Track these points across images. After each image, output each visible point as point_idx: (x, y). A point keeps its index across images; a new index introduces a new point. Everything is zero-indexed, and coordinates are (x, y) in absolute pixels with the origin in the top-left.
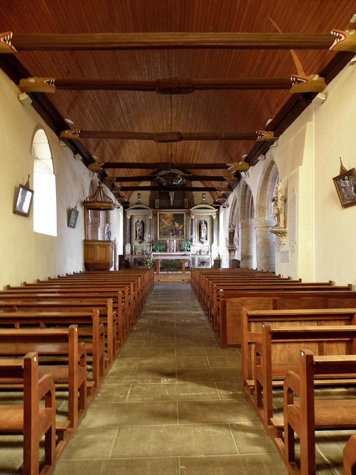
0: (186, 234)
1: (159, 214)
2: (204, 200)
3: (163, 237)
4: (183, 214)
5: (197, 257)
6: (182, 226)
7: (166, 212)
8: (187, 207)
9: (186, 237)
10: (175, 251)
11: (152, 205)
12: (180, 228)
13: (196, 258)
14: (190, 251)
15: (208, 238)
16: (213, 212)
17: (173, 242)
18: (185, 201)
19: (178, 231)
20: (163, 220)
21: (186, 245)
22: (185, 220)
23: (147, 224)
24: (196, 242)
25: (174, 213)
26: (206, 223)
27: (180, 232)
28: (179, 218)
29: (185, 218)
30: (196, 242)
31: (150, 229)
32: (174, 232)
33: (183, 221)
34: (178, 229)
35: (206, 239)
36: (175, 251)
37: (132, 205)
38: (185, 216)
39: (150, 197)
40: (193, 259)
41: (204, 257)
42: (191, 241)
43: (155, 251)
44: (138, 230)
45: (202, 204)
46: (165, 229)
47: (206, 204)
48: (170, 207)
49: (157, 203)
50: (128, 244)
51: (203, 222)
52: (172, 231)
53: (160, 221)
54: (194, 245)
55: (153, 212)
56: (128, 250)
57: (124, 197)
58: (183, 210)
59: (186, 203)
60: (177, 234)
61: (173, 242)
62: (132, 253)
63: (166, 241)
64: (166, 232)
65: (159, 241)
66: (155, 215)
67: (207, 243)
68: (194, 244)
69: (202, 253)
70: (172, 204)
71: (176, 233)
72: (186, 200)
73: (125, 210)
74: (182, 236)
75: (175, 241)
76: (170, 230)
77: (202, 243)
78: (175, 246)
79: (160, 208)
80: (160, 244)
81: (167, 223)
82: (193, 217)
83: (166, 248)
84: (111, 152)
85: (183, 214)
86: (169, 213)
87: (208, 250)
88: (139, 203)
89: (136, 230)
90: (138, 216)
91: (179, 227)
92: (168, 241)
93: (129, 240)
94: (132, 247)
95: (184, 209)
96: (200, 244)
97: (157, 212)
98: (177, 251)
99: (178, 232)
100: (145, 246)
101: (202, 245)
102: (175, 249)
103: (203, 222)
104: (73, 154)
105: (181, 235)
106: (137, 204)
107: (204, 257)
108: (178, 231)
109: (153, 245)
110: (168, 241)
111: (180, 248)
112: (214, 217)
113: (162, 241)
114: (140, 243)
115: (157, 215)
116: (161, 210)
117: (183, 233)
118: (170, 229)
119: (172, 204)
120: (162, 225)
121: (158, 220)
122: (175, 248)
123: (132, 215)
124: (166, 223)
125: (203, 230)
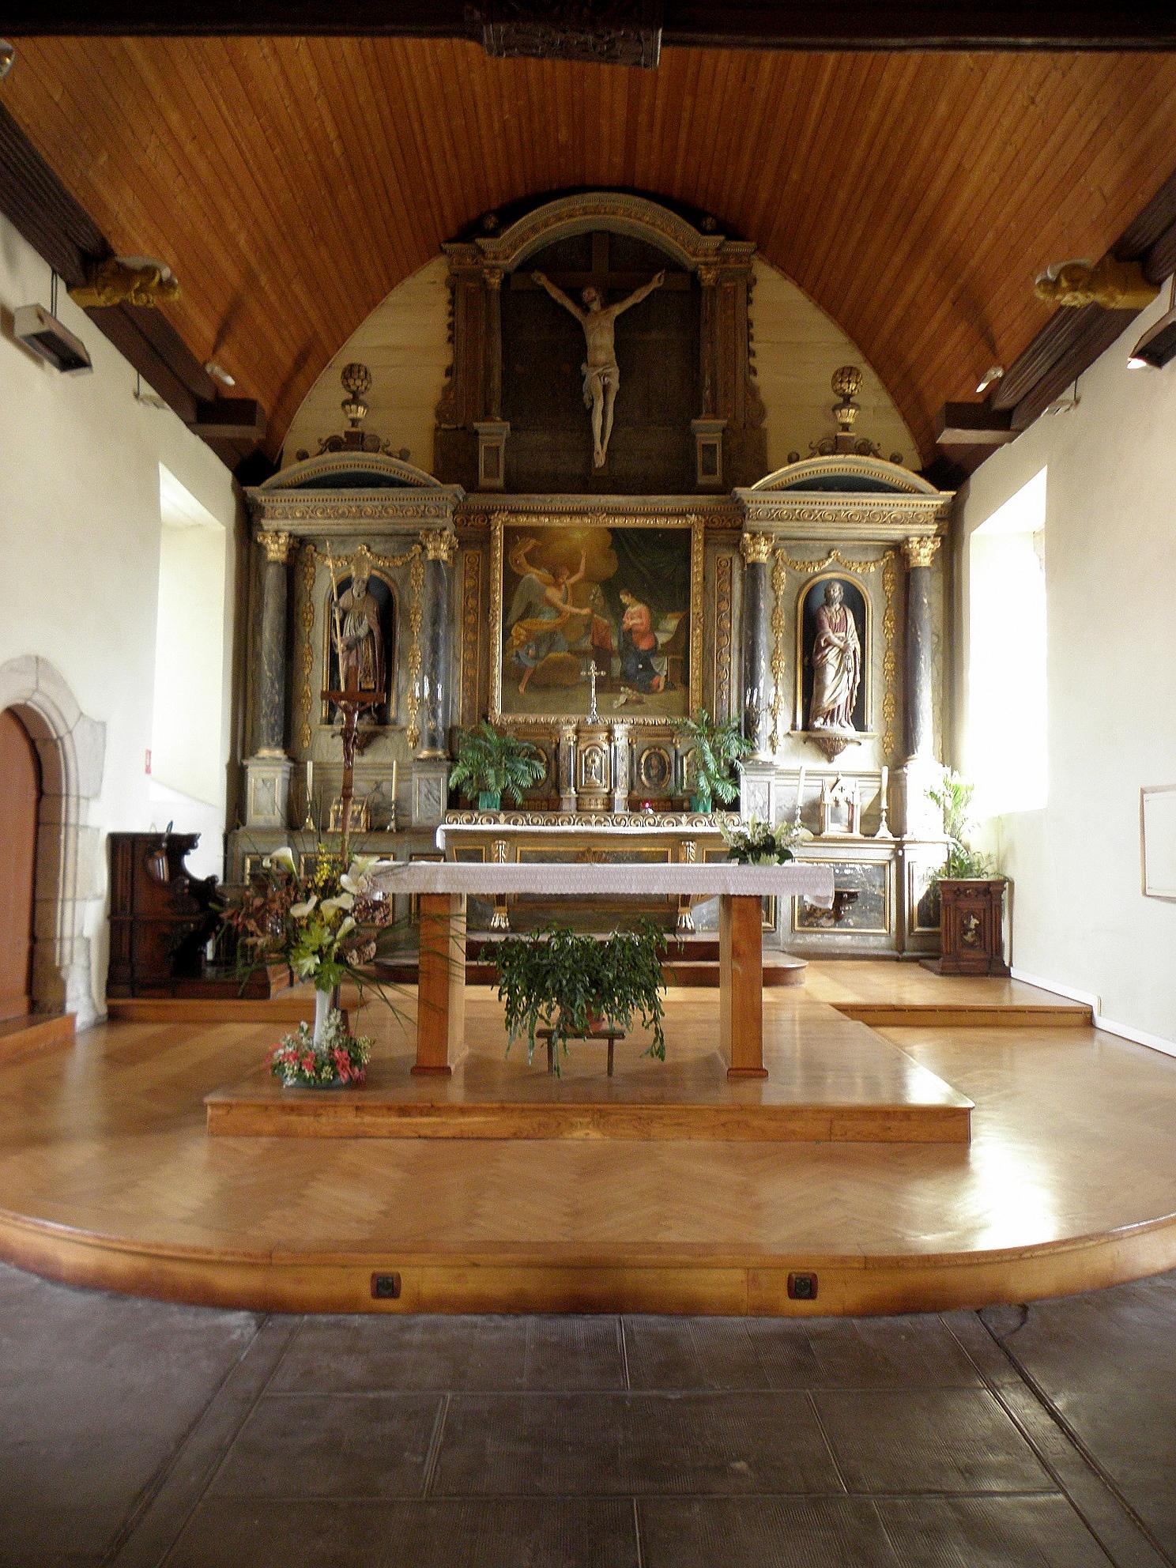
0: (706, 686)
1: (508, 531)
2: (849, 416)
3: (535, 698)
4: (687, 533)
6: (671, 624)
7: (560, 513)
8: (716, 479)
9: (706, 704)
10: (620, 809)
11: (455, 459)
12: (663, 638)
14: (734, 806)
15: (873, 714)
16: (910, 514)
17: (609, 741)
18: (702, 439)
19: (645, 658)
20: (534, 575)
21: (709, 757)
22: (696, 578)
23: (417, 601)
24: (783, 743)
25: (619, 522)
26: (855, 601)
27: (662, 667)
28: (652, 567)
29: (697, 558)
30: (783, 743)
31: (435, 641)
32: (617, 665)
33: (686, 585)
34: (644, 645)
35: (859, 722)
36: (620, 809)
37: (303, 456)
38: (697, 547)
39: (439, 414)
41: (842, 854)
42: (748, 728)
43: (472, 806)
44: (349, 648)
45: (837, 446)
46: (549, 639)
47: (865, 449)
48: (589, 483)
49: (493, 451)
50: (264, 752)
51: (837, 592)
52: (602, 656)
53: (512, 580)
54: (766, 767)
55: (462, 514)
57: (149, 271)
58: (686, 501)
59: (710, 449)
60: (639, 679)
61: (609, 741)
62: (293, 823)
63: (553, 730)
64: (559, 665)
65: (501, 731)
66: (473, 538)
67: (862, 754)
68: (763, 754)
69: (832, 829)
70: (600, 460)
71: (630, 672)
72: (708, 430)
73: (251, 490)
74: (676, 695)
75: (620, 731)
76: (583, 654)
77: (828, 748)
78: (622, 768)
79: (513, 487)
80: (510, 752)
81: (562, 601)
82: (761, 552)
83: (557, 784)
84: (242, 239)
85: (687, 533)
86: (581, 523)
87: (868, 800)
88: (355, 440)
89: (332, 646)
90: (341, 537)
91: (654, 627)
92: (569, 733)
93: (276, 718)
94: (297, 775)
95: (691, 489)
96: (810, 761)
97: (487, 513)
98: (634, 805)
99: (648, 667)
100: (402, 769)
101: (822, 765)
102: (620, 795)
103: (837, 592)
104: (226, 476)
105: (670, 686)
106: (334, 445)
107: (842, 854)
108: (645, 658)
109: (453, 759)
110: (569, 733)
111: (662, 788)
112: (924, 555)
113: (522, 730)
115: (487, 539)
116: (520, 501)
117: (680, 676)
118: (586, 644)
119: (600, 460)
120: (529, 611)
121: (498, 575)
123: (302, 529)
124: (553, 594)
125: (832, 655)
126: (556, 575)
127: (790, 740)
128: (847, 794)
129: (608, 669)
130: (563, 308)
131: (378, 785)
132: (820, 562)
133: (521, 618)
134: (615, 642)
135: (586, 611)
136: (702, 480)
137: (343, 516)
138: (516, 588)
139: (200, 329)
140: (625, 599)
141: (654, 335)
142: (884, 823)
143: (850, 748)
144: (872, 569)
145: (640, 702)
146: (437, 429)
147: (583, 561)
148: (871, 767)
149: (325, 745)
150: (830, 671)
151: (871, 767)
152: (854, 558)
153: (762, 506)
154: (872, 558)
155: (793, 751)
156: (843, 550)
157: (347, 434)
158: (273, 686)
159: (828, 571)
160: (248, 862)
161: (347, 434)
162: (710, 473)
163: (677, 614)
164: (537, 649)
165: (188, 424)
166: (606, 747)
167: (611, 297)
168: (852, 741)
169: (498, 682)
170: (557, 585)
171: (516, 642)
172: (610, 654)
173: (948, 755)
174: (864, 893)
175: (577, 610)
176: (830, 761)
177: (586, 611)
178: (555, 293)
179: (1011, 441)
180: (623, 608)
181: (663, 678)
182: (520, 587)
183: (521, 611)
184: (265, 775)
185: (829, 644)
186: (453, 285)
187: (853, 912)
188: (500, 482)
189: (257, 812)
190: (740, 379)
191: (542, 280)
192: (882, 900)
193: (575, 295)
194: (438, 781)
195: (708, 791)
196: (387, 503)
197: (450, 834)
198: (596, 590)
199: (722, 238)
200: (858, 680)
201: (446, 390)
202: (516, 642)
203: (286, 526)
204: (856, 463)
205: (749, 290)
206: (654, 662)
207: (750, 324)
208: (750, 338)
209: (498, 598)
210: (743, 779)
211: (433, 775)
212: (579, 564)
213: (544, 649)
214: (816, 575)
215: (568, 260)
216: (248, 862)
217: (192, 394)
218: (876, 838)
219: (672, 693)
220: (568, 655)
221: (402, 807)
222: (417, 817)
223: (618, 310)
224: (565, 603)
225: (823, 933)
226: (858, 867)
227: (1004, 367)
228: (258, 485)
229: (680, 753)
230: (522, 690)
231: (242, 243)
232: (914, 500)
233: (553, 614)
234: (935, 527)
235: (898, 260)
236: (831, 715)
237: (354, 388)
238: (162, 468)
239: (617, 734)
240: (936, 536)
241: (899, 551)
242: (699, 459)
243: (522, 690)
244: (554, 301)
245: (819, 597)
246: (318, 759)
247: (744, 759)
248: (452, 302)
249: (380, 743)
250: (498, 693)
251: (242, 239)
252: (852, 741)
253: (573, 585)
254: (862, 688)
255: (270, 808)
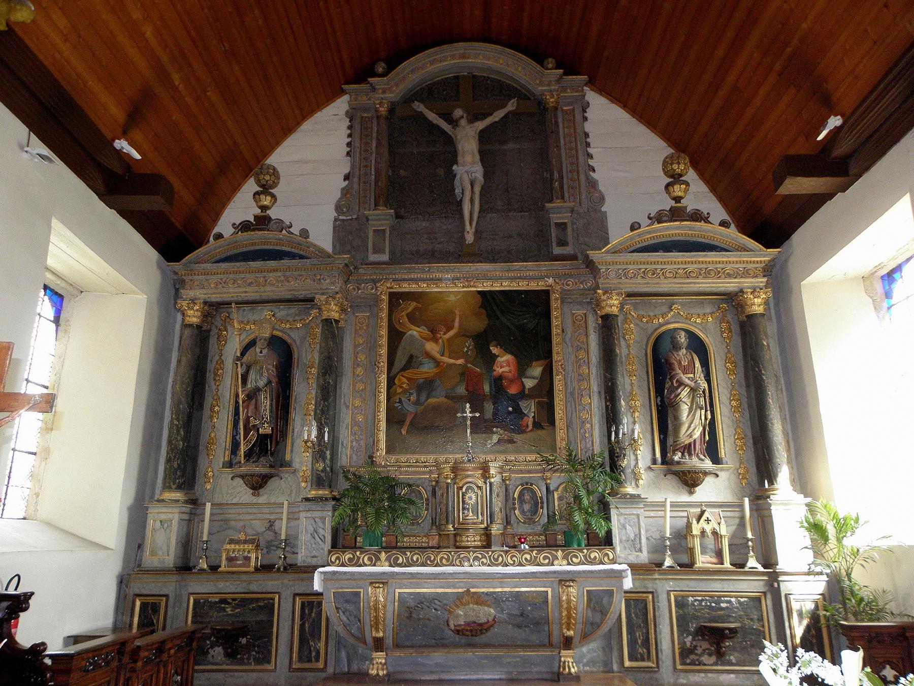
5: (667, 589)
6: (537, 370)
12: (529, 383)
13: (663, 597)
14: (608, 541)
15: (725, 448)
17: (484, 472)
18: (555, 218)
19: (514, 400)
20: (415, 332)
26: (699, 347)
27: (530, 408)
28: (150, 610)
32: (489, 407)
34: (513, 390)
39: (338, 208)
40: (639, 606)
46: (427, 386)
51: (682, 338)
54: (635, 498)
56: (161, 538)
64: (436, 408)
67: (716, 488)
70: (470, 238)
84: (149, 32)
91: (522, 371)
96: (672, 494)
99: (518, 412)
101: (685, 498)
103: (682, 338)
105: (537, 425)
108: (514, 400)
112: (757, 305)
114: (258, 484)
116: (401, 272)
117: (547, 410)
119: (470, 238)
120: (411, 362)
122: (499, 517)
124: (432, 348)
125: (684, 394)
126: (433, 331)
127: (651, 474)
128: (713, 524)
129: (482, 412)
130: (438, 127)
131: (271, 523)
132: (663, 315)
133: (404, 369)
134: (487, 388)
135: (460, 362)
136: (557, 251)
137: (250, 284)
138: (399, 343)
139: (106, 106)
140: (495, 350)
141: (511, 146)
142: (752, 553)
143: (709, 481)
144: (710, 319)
145: (511, 441)
146: (336, 220)
147: (457, 320)
148: (725, 496)
149: (225, 487)
150: (685, 409)
151: (725, 496)
152: (692, 311)
153: (611, 267)
154: (708, 311)
155: (654, 484)
156: (682, 304)
157: (256, 217)
158: (178, 431)
159: (678, 320)
160: (138, 603)
161: (256, 217)
162: (563, 245)
163: (541, 362)
164: (418, 395)
165: (101, 196)
166: (480, 483)
167: (474, 118)
168: (710, 473)
169: (383, 425)
170: (435, 340)
171: (399, 390)
172: (484, 398)
173: (803, 484)
174: (743, 627)
175: (452, 361)
176: (691, 493)
177: (460, 362)
178: (432, 116)
179: (844, 189)
180: (494, 357)
181: (531, 420)
182: (403, 343)
183: (404, 363)
184: (163, 517)
185: (681, 384)
186: (350, 115)
187: (734, 649)
188: (385, 257)
189: (153, 553)
190: (582, 178)
191: (420, 107)
192: (764, 632)
193: (447, 117)
194: (323, 519)
195: (582, 526)
196: (288, 274)
197: (327, 577)
198: (469, 343)
199: (561, 71)
200: (709, 417)
201: (345, 192)
202: (399, 390)
203: (200, 294)
204: (691, 229)
205: (584, 111)
206: (523, 404)
207: (587, 135)
208: (588, 145)
209: (384, 351)
210: (614, 513)
211: (317, 514)
212: (454, 321)
213: (423, 397)
214: (661, 325)
215: (443, 92)
216: (138, 603)
217: (99, 165)
218: (746, 569)
219: (540, 432)
220: (445, 400)
221: (290, 543)
222: (302, 557)
223: (481, 125)
224: (443, 355)
225: (706, 671)
226: (733, 600)
227: (842, 116)
228: (178, 261)
229: (552, 488)
230: (404, 432)
231: (148, 34)
232: (745, 257)
233: (432, 365)
234: (765, 280)
235: (720, 53)
236: (688, 449)
237: (263, 182)
238: (55, 223)
239: (492, 471)
240: (766, 287)
241: (733, 301)
242: (553, 235)
243: (404, 432)
244: (430, 123)
245: (666, 345)
246: (217, 500)
247: (613, 493)
248: (350, 127)
249: (273, 483)
250: (382, 436)
251: (149, 32)
252: (710, 473)
253: (448, 340)
254: (712, 424)
255: (165, 548)
